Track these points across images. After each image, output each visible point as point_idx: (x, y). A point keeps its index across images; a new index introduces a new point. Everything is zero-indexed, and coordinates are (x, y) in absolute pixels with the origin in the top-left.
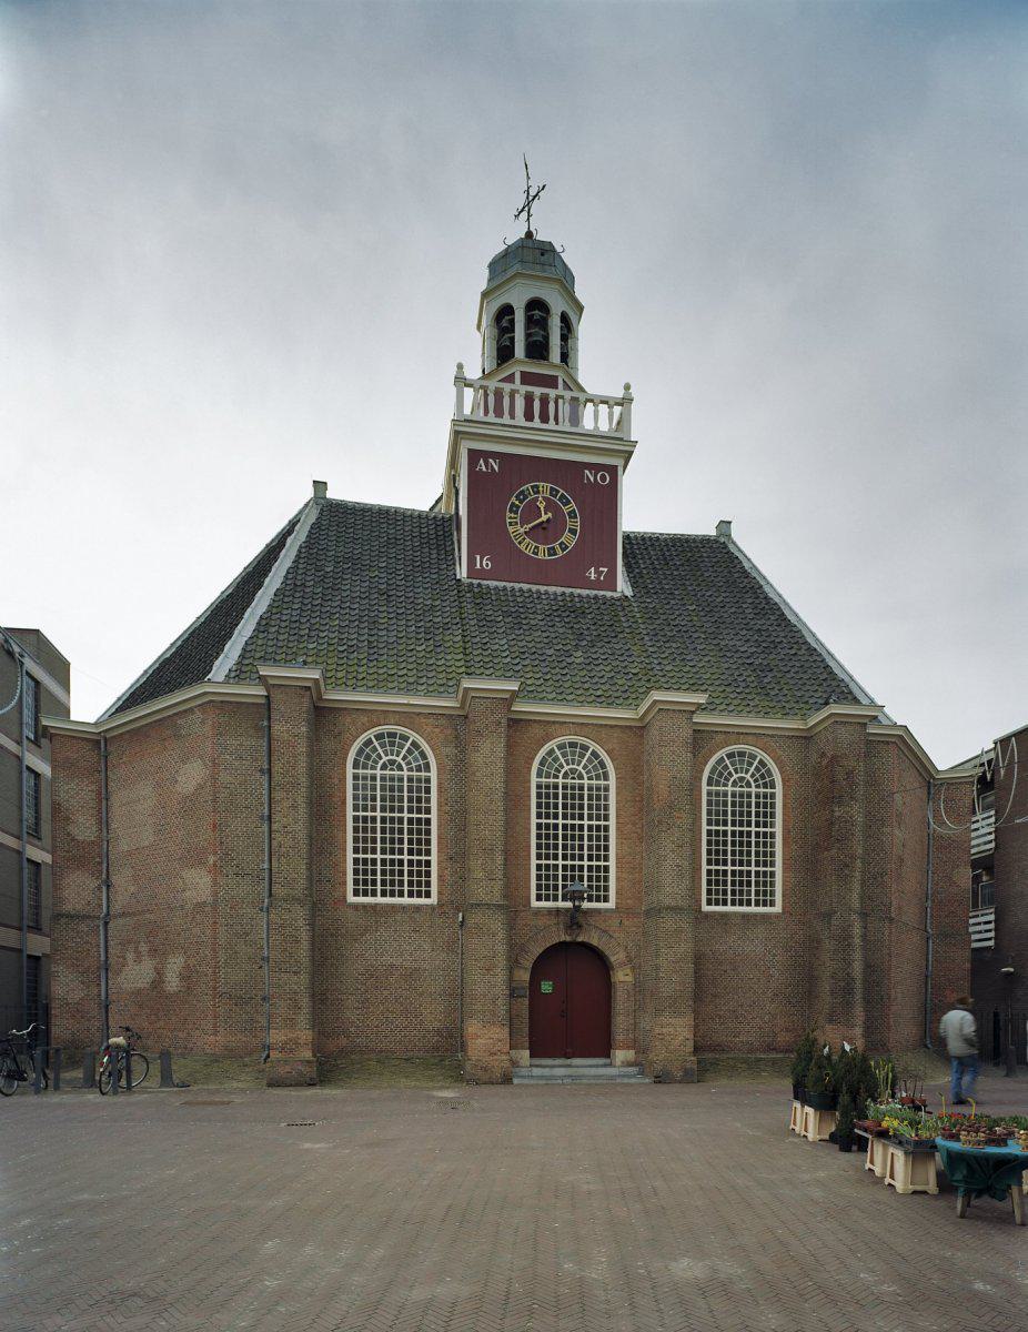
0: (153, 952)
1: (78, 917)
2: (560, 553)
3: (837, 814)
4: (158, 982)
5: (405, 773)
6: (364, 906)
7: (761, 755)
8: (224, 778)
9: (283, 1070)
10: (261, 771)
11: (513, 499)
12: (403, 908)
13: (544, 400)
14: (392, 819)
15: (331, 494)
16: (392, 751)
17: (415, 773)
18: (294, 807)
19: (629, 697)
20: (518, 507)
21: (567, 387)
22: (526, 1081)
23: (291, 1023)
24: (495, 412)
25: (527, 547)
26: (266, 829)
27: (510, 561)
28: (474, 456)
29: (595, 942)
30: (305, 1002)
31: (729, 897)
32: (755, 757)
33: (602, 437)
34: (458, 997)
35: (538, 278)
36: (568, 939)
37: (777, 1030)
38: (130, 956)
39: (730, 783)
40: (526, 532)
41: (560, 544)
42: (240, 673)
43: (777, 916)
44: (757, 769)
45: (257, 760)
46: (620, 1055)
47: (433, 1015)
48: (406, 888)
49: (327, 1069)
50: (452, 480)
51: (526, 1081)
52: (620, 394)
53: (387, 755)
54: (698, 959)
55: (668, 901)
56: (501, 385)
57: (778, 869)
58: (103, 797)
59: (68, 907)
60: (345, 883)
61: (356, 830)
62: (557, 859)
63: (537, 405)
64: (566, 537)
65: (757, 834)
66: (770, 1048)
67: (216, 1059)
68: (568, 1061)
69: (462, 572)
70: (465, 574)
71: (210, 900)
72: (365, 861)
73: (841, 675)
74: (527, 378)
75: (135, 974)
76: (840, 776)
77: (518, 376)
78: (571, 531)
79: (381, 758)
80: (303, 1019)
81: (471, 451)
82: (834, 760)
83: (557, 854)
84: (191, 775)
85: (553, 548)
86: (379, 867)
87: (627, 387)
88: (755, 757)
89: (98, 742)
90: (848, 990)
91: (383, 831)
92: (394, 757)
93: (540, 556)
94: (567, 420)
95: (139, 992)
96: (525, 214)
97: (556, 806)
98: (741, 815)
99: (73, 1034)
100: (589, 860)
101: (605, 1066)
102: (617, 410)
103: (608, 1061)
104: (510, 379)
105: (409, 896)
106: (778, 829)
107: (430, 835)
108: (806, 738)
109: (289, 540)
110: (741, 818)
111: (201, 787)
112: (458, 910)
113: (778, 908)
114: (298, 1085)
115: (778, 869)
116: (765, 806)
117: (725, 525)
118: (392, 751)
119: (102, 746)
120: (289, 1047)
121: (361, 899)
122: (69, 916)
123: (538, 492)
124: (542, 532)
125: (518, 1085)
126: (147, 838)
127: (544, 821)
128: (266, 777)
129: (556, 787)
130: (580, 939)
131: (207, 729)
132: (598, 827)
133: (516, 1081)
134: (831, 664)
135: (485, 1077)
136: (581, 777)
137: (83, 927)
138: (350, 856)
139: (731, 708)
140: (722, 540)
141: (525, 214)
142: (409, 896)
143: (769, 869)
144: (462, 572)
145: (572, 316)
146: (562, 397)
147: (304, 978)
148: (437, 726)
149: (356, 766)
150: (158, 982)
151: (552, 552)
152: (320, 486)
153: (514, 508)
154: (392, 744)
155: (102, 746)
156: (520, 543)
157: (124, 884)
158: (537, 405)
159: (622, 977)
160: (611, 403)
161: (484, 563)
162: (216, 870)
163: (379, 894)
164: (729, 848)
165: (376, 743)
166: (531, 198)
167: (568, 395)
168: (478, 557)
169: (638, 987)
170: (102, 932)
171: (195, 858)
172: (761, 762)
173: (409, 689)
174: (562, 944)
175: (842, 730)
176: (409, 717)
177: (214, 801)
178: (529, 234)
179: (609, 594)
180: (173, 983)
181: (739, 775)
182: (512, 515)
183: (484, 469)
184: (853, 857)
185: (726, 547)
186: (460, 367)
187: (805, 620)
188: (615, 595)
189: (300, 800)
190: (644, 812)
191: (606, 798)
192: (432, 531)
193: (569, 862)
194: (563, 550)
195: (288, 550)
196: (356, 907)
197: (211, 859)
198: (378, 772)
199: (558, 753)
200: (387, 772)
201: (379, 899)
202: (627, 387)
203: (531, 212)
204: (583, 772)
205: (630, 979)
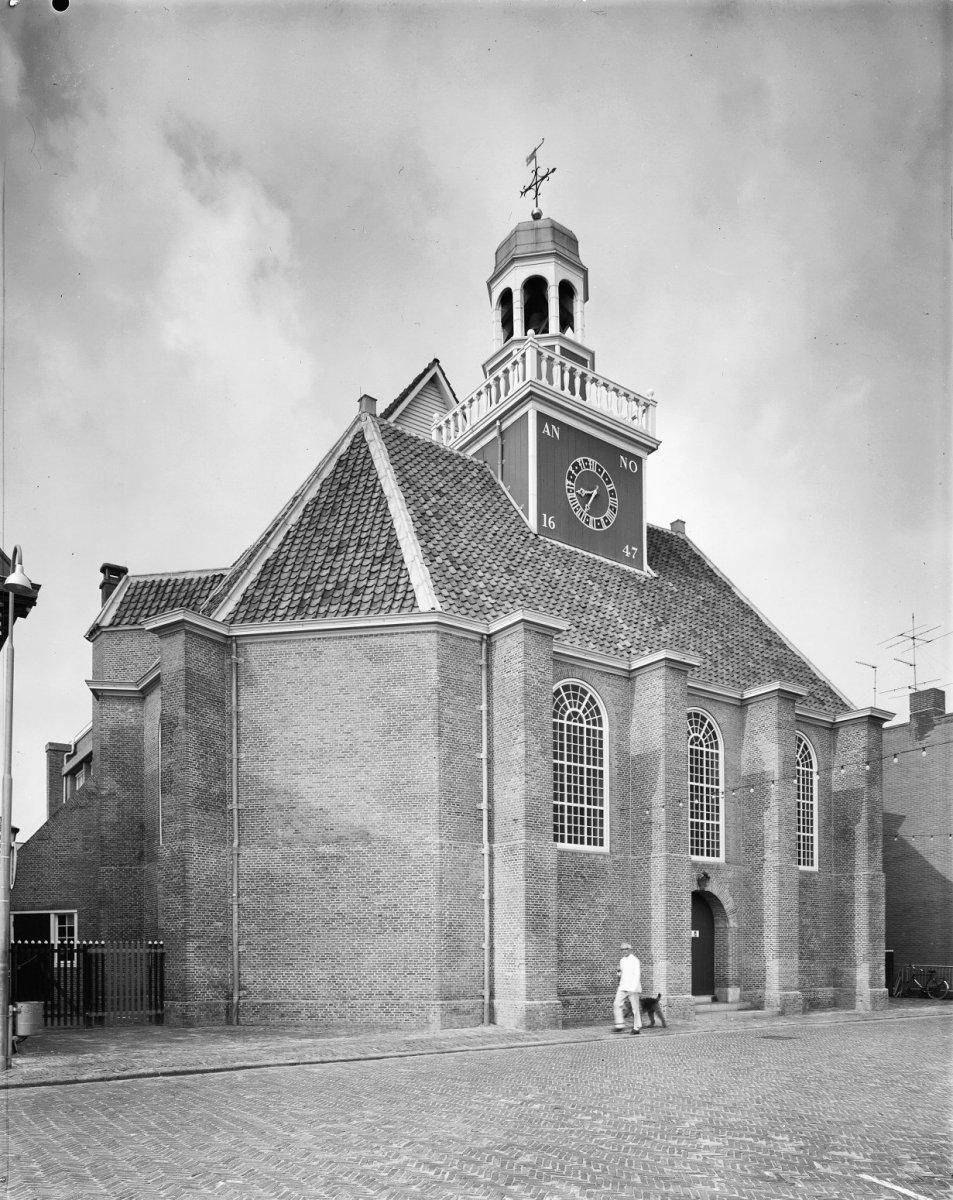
2: (605, 527)
13: (583, 376)
25: (581, 513)
28: (542, 418)
44: (588, 706)
46: (733, 993)
79: (567, 709)
92: (576, 710)
93: (590, 526)
96: (532, 193)
125: (8, 1009)
141: (532, 193)
153: (571, 477)
156: (576, 510)
161: (550, 523)
166: (539, 178)
191: (601, 745)
203: (539, 192)
204: (583, 716)
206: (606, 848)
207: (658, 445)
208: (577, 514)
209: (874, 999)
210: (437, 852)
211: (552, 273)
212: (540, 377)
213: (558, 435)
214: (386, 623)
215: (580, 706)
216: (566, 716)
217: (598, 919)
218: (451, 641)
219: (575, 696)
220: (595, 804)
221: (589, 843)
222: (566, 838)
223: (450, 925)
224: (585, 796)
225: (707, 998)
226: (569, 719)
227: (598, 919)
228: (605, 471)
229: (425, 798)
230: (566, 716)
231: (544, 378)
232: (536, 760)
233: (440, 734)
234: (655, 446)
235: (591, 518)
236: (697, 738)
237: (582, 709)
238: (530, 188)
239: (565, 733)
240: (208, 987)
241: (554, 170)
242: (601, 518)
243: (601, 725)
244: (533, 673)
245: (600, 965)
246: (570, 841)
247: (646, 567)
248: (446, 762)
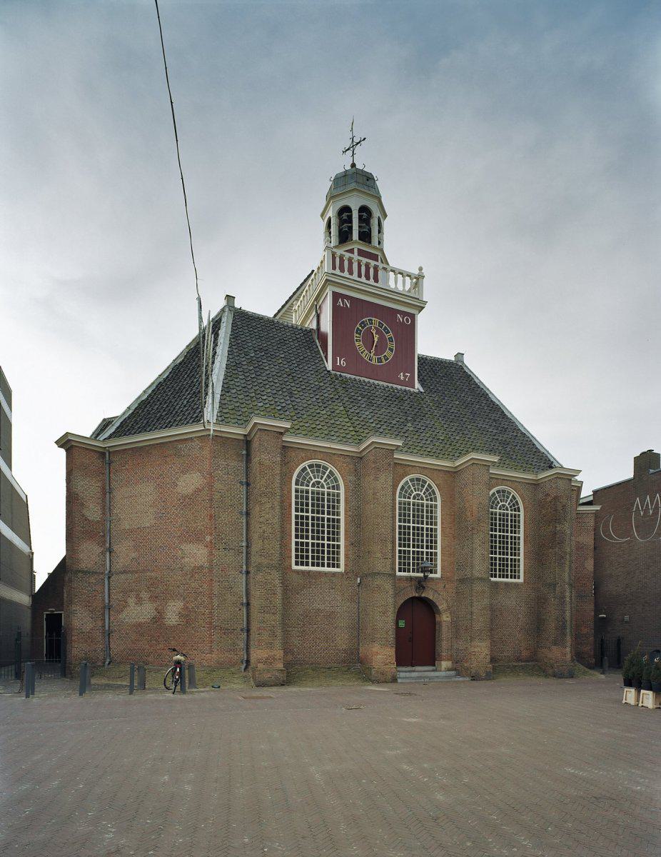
0: (154, 598)
1: (89, 573)
3: (558, 529)
4: (159, 618)
5: (326, 490)
6: (303, 572)
7: (513, 493)
8: (218, 485)
9: (266, 676)
10: (241, 483)
11: (358, 326)
12: (326, 574)
13: (376, 268)
15: (237, 305)
17: (331, 490)
18: (272, 508)
19: (454, 457)
20: (361, 331)
22: (404, 681)
23: (270, 646)
25: (365, 355)
26: (244, 521)
27: (356, 363)
28: (336, 296)
29: (431, 598)
30: (279, 632)
32: (326, 469)
33: (390, 291)
34: (359, 630)
35: (364, 193)
36: (417, 595)
37: (522, 649)
38: (131, 601)
43: (521, 584)
44: (511, 501)
45: (238, 475)
46: (445, 664)
47: (342, 641)
48: (326, 561)
49: (291, 674)
51: (404, 681)
52: (416, 272)
53: (315, 478)
54: (492, 609)
55: (477, 574)
56: (344, 253)
57: (522, 557)
58: (106, 493)
59: (83, 566)
60: (291, 557)
61: (297, 524)
62: (324, 540)
64: (387, 353)
65: (329, 520)
66: (518, 660)
67: (212, 670)
68: (414, 668)
71: (206, 565)
73: (542, 450)
74: (361, 253)
75: (138, 612)
76: (560, 508)
77: (356, 251)
78: (390, 349)
80: (278, 643)
82: (556, 498)
83: (308, 536)
84: (190, 482)
87: (421, 269)
88: (326, 469)
89: (104, 454)
90: (564, 627)
92: (319, 480)
93: (373, 362)
95: (140, 625)
97: (323, 506)
98: (318, 506)
99: (86, 654)
101: (433, 671)
103: (434, 668)
104: (351, 251)
106: (522, 535)
108: (536, 485)
111: (198, 491)
112: (357, 576)
113: (521, 580)
114: (276, 685)
115: (342, 543)
119: (107, 456)
120: (269, 661)
121: (300, 568)
122: (83, 572)
123: (372, 324)
126: (148, 521)
127: (300, 514)
128: (245, 487)
129: (307, 492)
130: (423, 595)
131: (206, 452)
133: (399, 681)
134: (535, 443)
135: (383, 679)
136: (323, 487)
137: (92, 580)
138: (294, 540)
139: (323, 435)
141: (350, 153)
143: (336, 543)
144: (329, 366)
147: (278, 617)
148: (344, 463)
150: (159, 618)
151: (380, 360)
152: (230, 299)
153: (358, 332)
155: (107, 456)
156: (362, 353)
157: (125, 553)
159: (445, 618)
160: (397, 272)
162: (211, 546)
163: (310, 564)
164: (326, 529)
166: (354, 144)
169: (455, 625)
170: (106, 582)
171: (196, 537)
172: (429, 485)
173: (327, 437)
174: (413, 598)
175: (560, 483)
176: (329, 455)
177: (211, 500)
178: (353, 165)
179: (412, 390)
180: (172, 618)
182: (358, 335)
183: (342, 305)
184: (565, 553)
185: (463, 369)
187: (516, 417)
189: (276, 503)
190: (457, 518)
191: (519, 522)
194: (386, 360)
196: (298, 572)
197: (208, 538)
198: (411, 500)
200: (315, 489)
201: (310, 568)
202: (421, 269)
204: (424, 496)
205: (449, 619)
206: (342, 569)
208: (363, 355)
211: (355, 203)
212: (334, 268)
215: (507, 501)
216: (412, 497)
219: (318, 471)
220: (515, 556)
221: (511, 578)
222: (326, 564)
224: (509, 551)
226: (414, 498)
230: (412, 497)
231: (363, 276)
236: (504, 506)
237: (323, 479)
238: (348, 149)
239: (510, 518)
241: (364, 139)
243: (519, 511)
246: (500, 577)
247: (417, 385)
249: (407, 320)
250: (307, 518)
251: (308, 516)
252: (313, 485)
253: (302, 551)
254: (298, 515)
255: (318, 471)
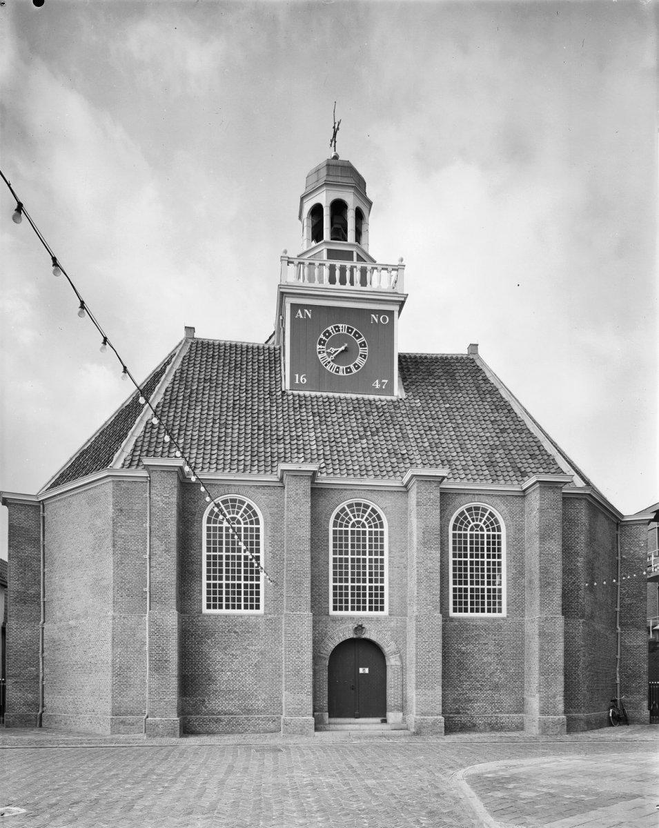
2: (355, 371)
13: (343, 269)
14: (477, 563)
15: (198, 335)
16: (358, 515)
21: (360, 259)
24: (350, 282)
25: (331, 368)
27: (320, 378)
28: (295, 307)
31: (469, 606)
36: (355, 637)
39: (469, 529)
40: (332, 361)
41: (354, 365)
42: (131, 463)
50: (281, 322)
61: (208, 564)
63: (338, 273)
64: (358, 360)
69: (286, 385)
70: (288, 387)
72: (460, 590)
74: (332, 254)
79: (237, 514)
81: (292, 305)
85: (349, 368)
86: (469, 593)
91: (227, 564)
93: (341, 373)
94: (306, 279)
100: (352, 582)
102: (394, 273)
105: (369, 610)
107: (207, 569)
109: (168, 368)
110: (478, 551)
116: (494, 543)
117: (474, 347)
118: (358, 515)
124: (342, 357)
127: (457, 559)
132: (376, 560)
140: (471, 357)
142: (369, 610)
144: (286, 385)
145: (365, 210)
146: (356, 267)
148: (264, 494)
149: (454, 528)
151: (348, 370)
152: (190, 329)
153: (322, 342)
154: (233, 507)
158: (338, 273)
159: (392, 662)
160: (390, 268)
161: (302, 379)
165: (467, 514)
167: (359, 265)
168: (297, 375)
172: (491, 514)
179: (389, 398)
181: (475, 523)
182: (321, 347)
183: (301, 317)
186: (285, 252)
188: (394, 399)
192: (267, 358)
193: (344, 584)
195: (167, 376)
199: (348, 510)
207: (405, 298)
209: (545, 728)
210: (111, 621)
213: (310, 316)
214: (90, 481)
217: (250, 662)
218: (124, 485)
223: (120, 668)
225: (378, 720)
227: (250, 662)
228: (355, 330)
229: (107, 588)
232: (160, 557)
233: (114, 546)
234: (403, 299)
235: (341, 367)
240: (24, 705)
242: (352, 366)
244: (159, 499)
245: (252, 694)
248: (118, 564)
249: (384, 319)
250: (466, 563)
251: (351, 555)
252: (353, 526)
253: (215, 593)
254: (354, 559)
255: (233, 507)
